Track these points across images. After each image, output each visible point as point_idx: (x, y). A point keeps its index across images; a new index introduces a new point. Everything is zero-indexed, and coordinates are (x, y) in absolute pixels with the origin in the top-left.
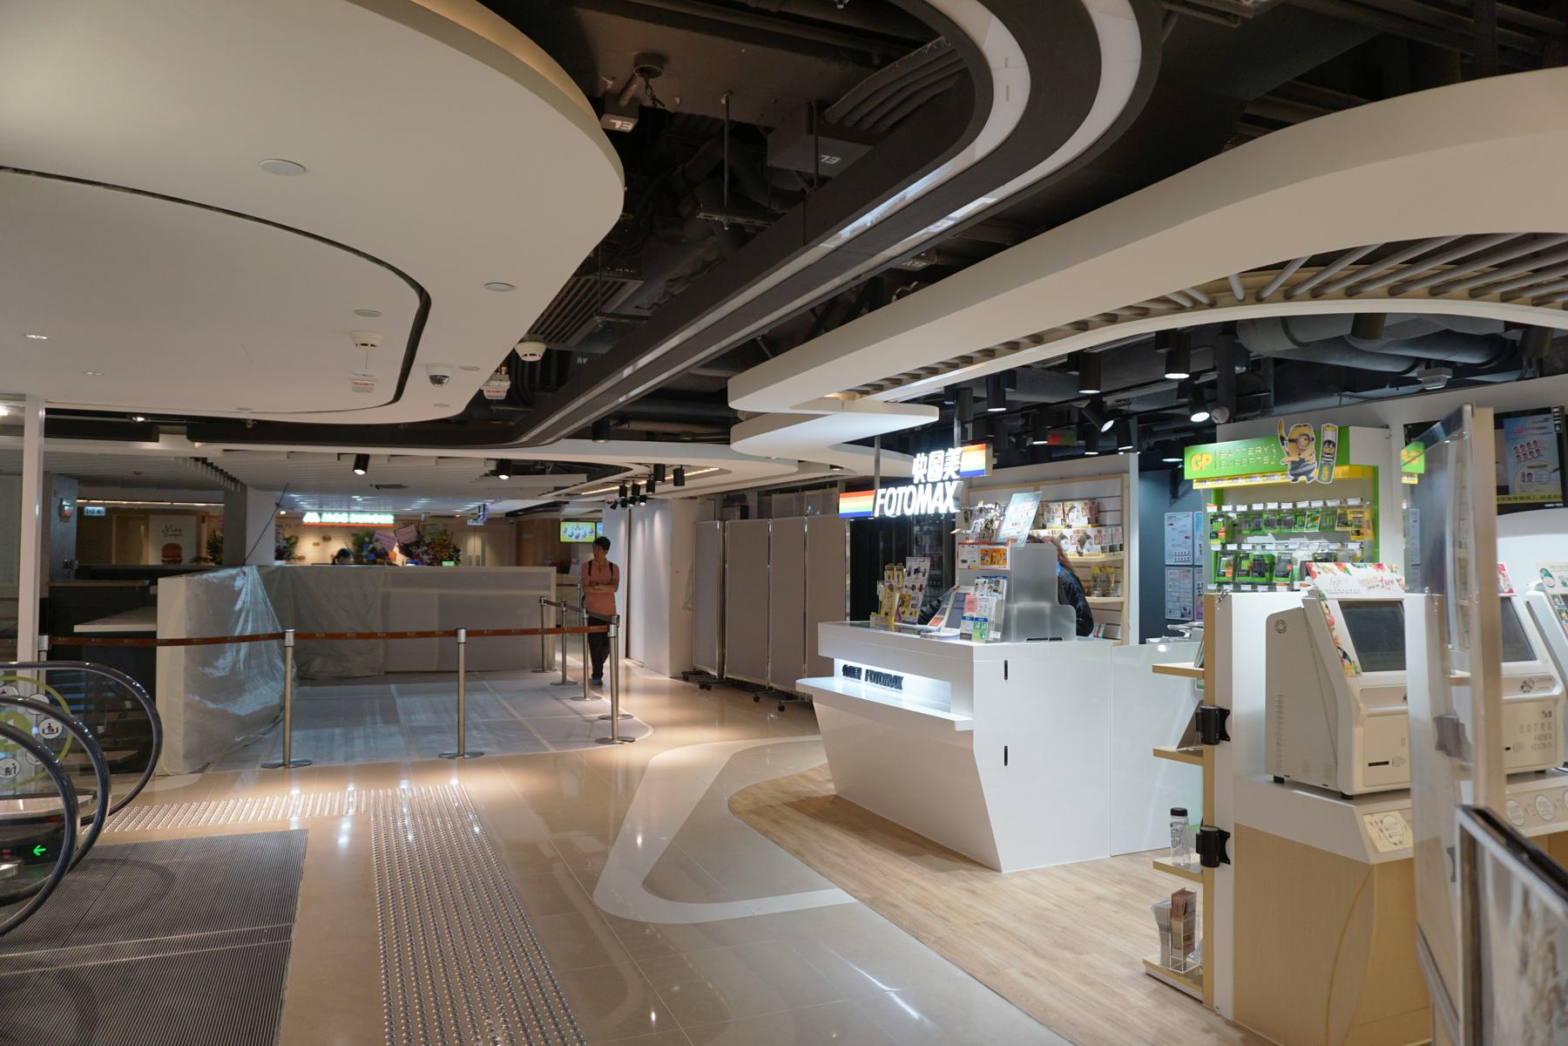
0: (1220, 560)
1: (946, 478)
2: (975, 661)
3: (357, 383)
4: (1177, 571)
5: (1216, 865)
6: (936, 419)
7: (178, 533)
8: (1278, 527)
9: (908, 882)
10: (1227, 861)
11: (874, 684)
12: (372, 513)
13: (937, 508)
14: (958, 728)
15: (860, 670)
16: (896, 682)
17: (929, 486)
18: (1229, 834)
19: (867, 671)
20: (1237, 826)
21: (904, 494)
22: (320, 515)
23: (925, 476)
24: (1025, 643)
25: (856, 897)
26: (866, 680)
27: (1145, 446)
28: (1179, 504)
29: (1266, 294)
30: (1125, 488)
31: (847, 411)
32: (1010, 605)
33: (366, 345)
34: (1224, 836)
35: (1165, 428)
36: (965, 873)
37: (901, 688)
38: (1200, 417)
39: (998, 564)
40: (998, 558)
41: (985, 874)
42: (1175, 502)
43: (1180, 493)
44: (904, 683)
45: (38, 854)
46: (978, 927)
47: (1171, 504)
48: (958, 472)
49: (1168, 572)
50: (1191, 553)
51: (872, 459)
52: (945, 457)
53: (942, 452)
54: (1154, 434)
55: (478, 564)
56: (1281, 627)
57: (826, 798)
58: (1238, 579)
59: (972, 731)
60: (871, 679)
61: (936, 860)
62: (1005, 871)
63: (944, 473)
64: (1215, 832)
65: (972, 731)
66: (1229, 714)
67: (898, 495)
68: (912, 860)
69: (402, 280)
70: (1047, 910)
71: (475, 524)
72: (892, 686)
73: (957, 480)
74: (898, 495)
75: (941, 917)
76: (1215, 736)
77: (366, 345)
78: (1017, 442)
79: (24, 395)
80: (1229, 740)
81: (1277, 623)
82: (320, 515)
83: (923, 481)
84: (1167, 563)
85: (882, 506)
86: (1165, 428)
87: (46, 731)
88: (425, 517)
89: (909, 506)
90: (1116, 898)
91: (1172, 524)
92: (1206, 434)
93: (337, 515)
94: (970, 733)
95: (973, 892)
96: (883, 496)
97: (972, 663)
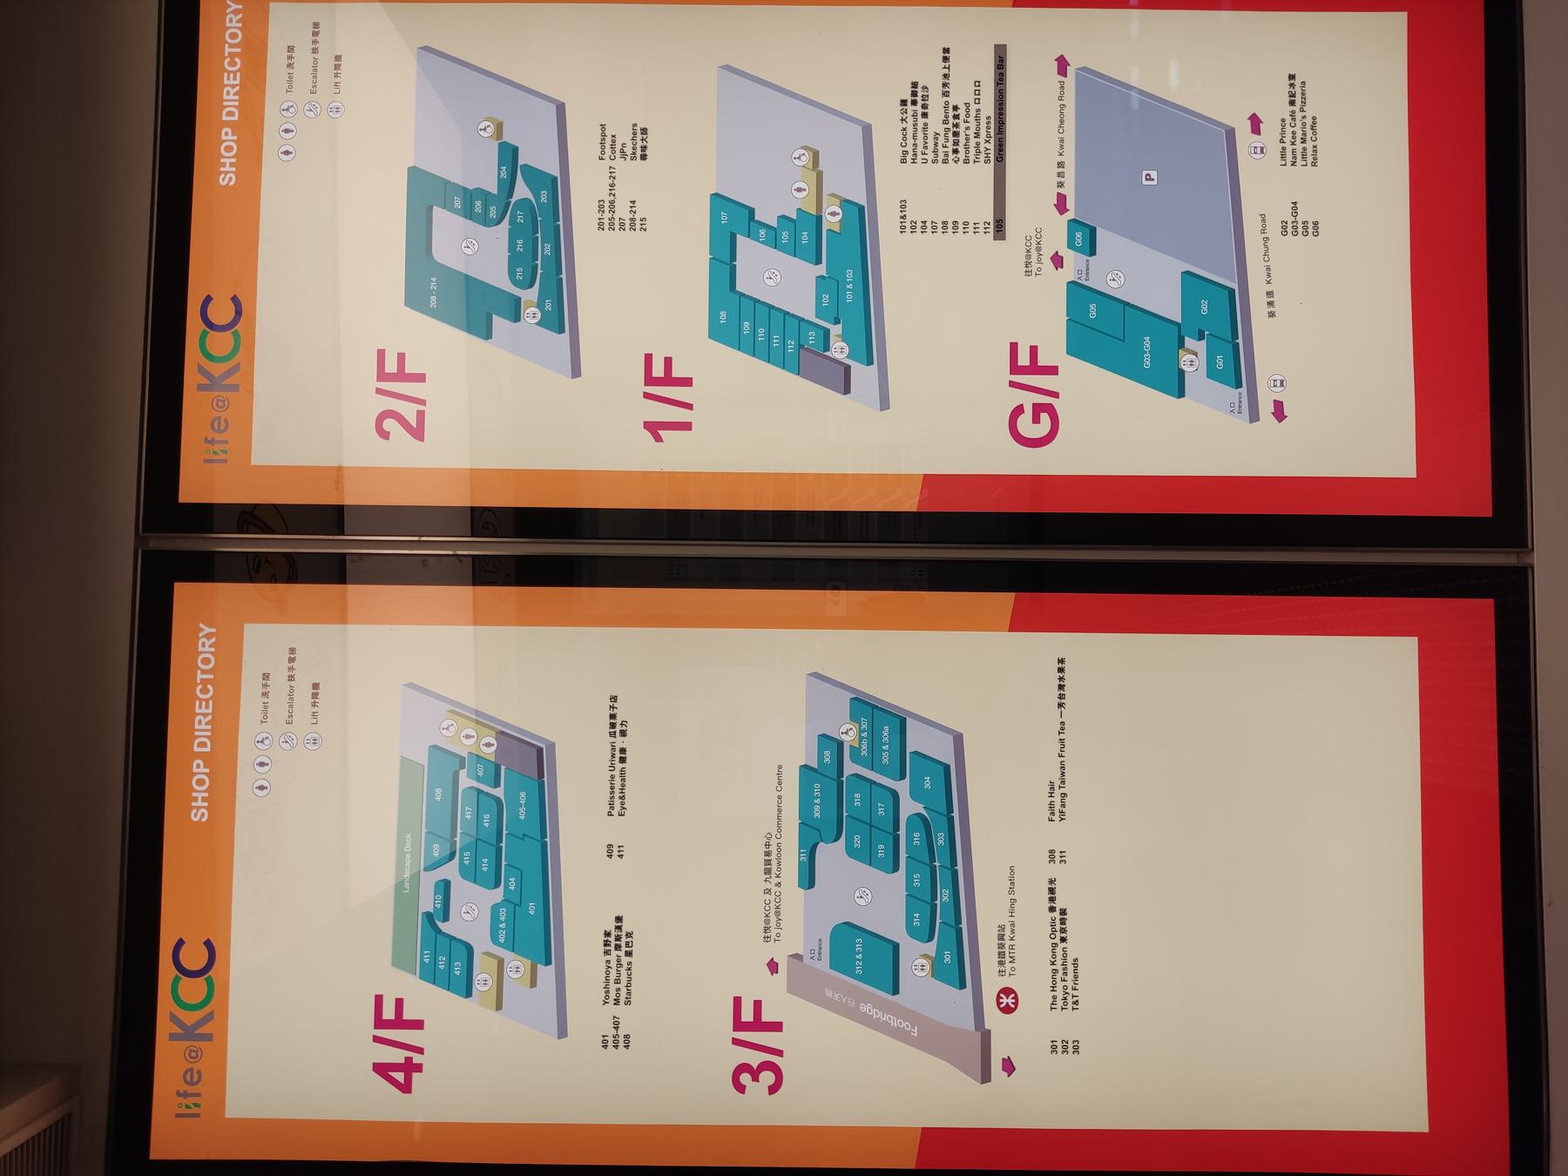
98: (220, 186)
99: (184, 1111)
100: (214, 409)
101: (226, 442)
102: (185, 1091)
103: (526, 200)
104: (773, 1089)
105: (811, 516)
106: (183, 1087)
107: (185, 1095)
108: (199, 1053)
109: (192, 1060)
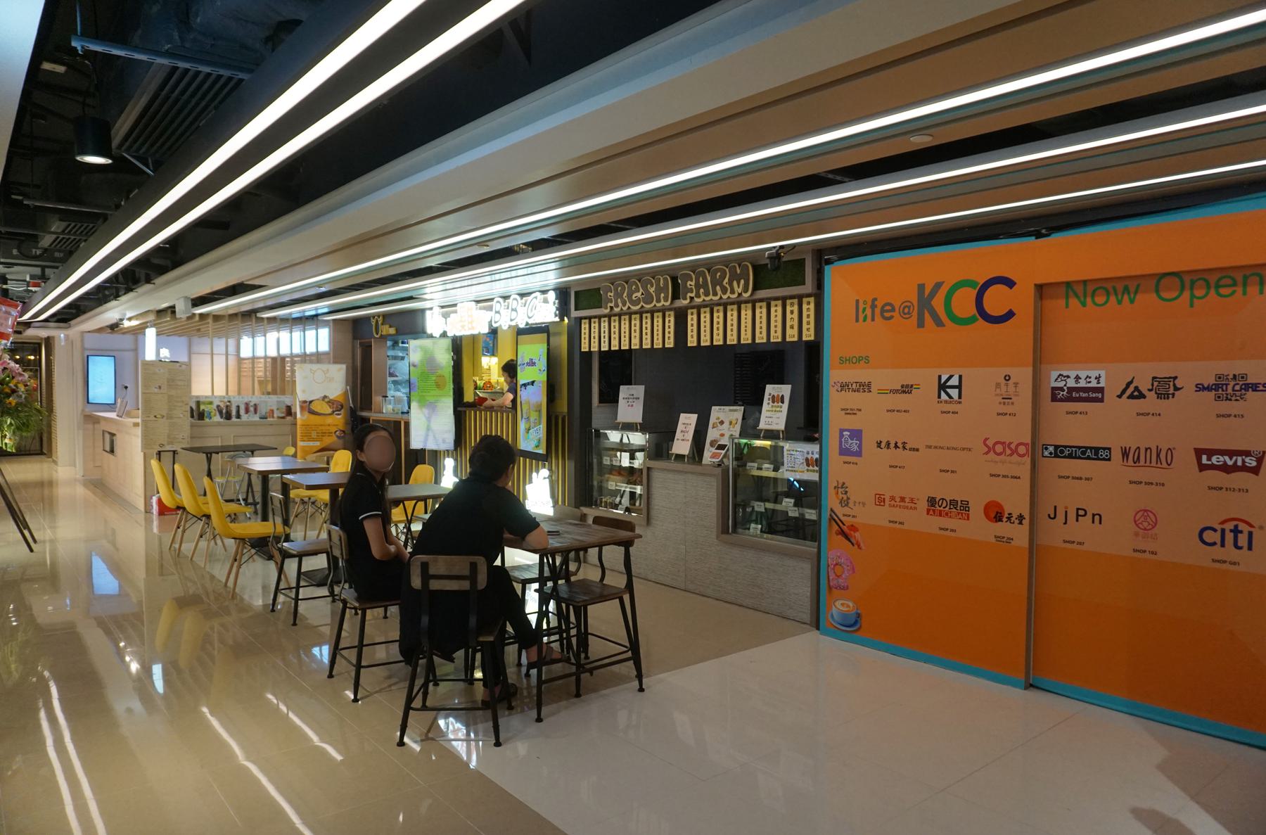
59: (924, 284)
98: (504, 330)
99: (861, 306)
100: (906, 302)
101: (873, 320)
102: (876, 306)
103: (390, 545)
104: (1049, 515)
105: (1031, 509)
106: (879, 304)
107: (873, 306)
108: (907, 316)
109: (902, 306)
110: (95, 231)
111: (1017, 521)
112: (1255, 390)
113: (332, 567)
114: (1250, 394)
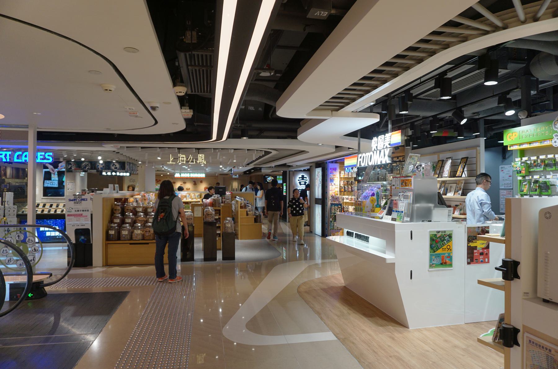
0: (523, 184)
1: (385, 147)
2: (396, 231)
3: (130, 113)
4: (505, 191)
5: (512, 346)
6: (377, 120)
7: (134, 181)
8: (554, 167)
9: (364, 331)
10: (518, 344)
11: (358, 239)
12: (198, 173)
13: (381, 162)
14: (388, 262)
15: (353, 233)
16: (366, 239)
17: (378, 152)
18: (519, 330)
19: (356, 234)
20: (524, 326)
21: (368, 156)
22: (180, 174)
23: (377, 147)
24: (421, 223)
25: (337, 337)
26: (355, 238)
27: (489, 135)
28: (506, 161)
29: (540, 14)
30: (478, 153)
31: (334, 117)
32: (414, 205)
33: (107, 90)
34: (516, 331)
35: (499, 126)
36: (392, 328)
37: (368, 242)
38: (510, 113)
39: (408, 186)
40: (408, 183)
41: (401, 329)
42: (504, 161)
43: (507, 157)
44: (370, 239)
45: (30, 296)
46: (390, 359)
47: (502, 162)
48: (390, 144)
49: (501, 191)
50: (512, 183)
51: (357, 142)
52: (384, 138)
53: (383, 136)
54: (493, 130)
55: (236, 191)
56: (548, 215)
57: (340, 287)
58: (531, 193)
59: (395, 263)
60: (357, 237)
61: (381, 321)
62: (410, 329)
63: (384, 145)
64: (511, 329)
65: (395, 263)
66: (519, 264)
67: (366, 156)
68: (369, 319)
69: (92, 52)
70: (428, 351)
71: (235, 177)
72: (365, 241)
73: (389, 148)
74: (366, 156)
75: (374, 351)
76: (511, 276)
77: (107, 90)
78: (427, 135)
79: (28, 125)
80: (519, 279)
81: (546, 214)
82: (180, 174)
83: (376, 149)
84: (500, 188)
85: (360, 162)
86: (499, 126)
87: (34, 251)
88: (218, 175)
89: (370, 161)
90: (464, 347)
91: (503, 171)
92: (515, 123)
93: (186, 174)
94: (394, 264)
95: (393, 339)
96: (361, 158)
97: (395, 232)
110: (148, 244)
111: (149, 210)
112: (84, 201)
113: (458, 66)
114: (83, 201)
